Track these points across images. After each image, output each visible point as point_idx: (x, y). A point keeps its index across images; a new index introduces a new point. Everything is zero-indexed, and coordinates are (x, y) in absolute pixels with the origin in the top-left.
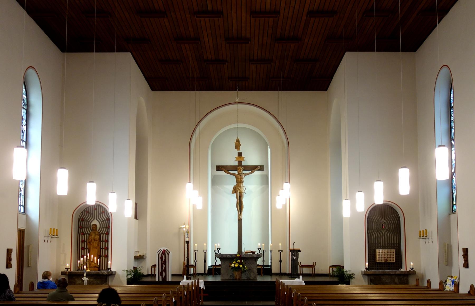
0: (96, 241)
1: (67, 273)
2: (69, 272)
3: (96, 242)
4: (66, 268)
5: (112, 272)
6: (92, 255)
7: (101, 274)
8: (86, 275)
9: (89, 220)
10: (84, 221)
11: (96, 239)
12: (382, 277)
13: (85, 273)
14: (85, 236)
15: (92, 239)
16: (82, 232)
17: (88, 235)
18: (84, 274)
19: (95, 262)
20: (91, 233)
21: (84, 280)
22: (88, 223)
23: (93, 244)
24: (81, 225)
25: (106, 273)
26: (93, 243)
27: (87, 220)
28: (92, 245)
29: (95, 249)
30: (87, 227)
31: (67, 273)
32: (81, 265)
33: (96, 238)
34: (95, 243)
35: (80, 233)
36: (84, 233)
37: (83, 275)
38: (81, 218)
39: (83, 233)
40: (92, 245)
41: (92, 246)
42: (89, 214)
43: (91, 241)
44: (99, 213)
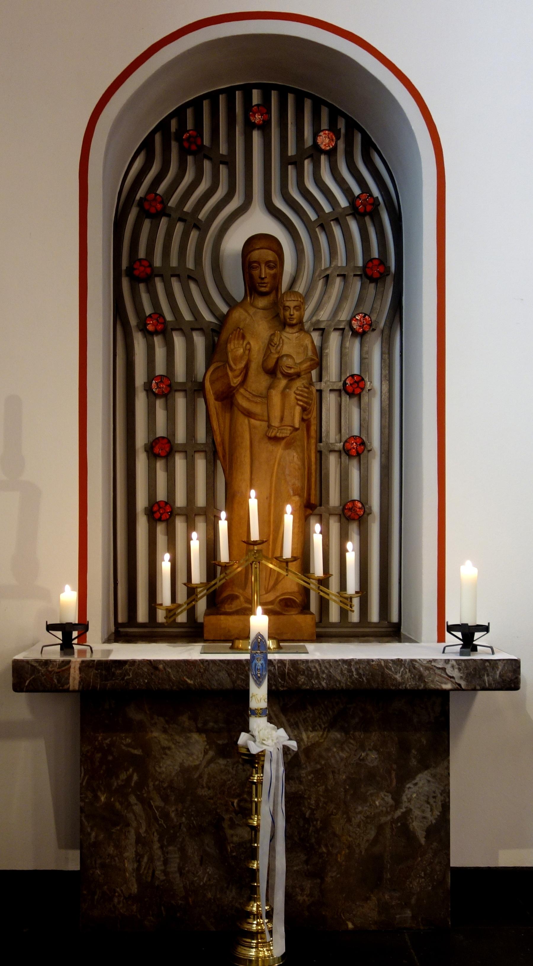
0: (291, 377)
1: (75, 676)
2: (86, 666)
3: (287, 387)
4: (50, 628)
5: (292, 557)
6: (288, 502)
7: (410, 684)
8: (271, 693)
9: (203, 215)
10: (164, 221)
11: (287, 362)
12: (318, 368)
13: (259, 684)
14: (179, 342)
15: (247, 368)
16: (148, 310)
17: (199, 341)
18: (253, 688)
19: (287, 553)
20: (238, 314)
21: (261, 755)
22: (313, 216)
23: (257, 409)
24: (142, 254)
25: (456, 673)
26: (266, 397)
27: (188, 207)
28: (249, 414)
29: (279, 450)
30: (190, 264)
31: (75, 676)
32: (192, 591)
33: (286, 349)
34: (284, 394)
35: (133, 321)
36: (169, 317)
37: (245, 695)
38: (141, 193)
39: (158, 314)
40: (249, 414)
41: (251, 428)
42: (207, 165)
43: (243, 382)
44: (291, 151)
